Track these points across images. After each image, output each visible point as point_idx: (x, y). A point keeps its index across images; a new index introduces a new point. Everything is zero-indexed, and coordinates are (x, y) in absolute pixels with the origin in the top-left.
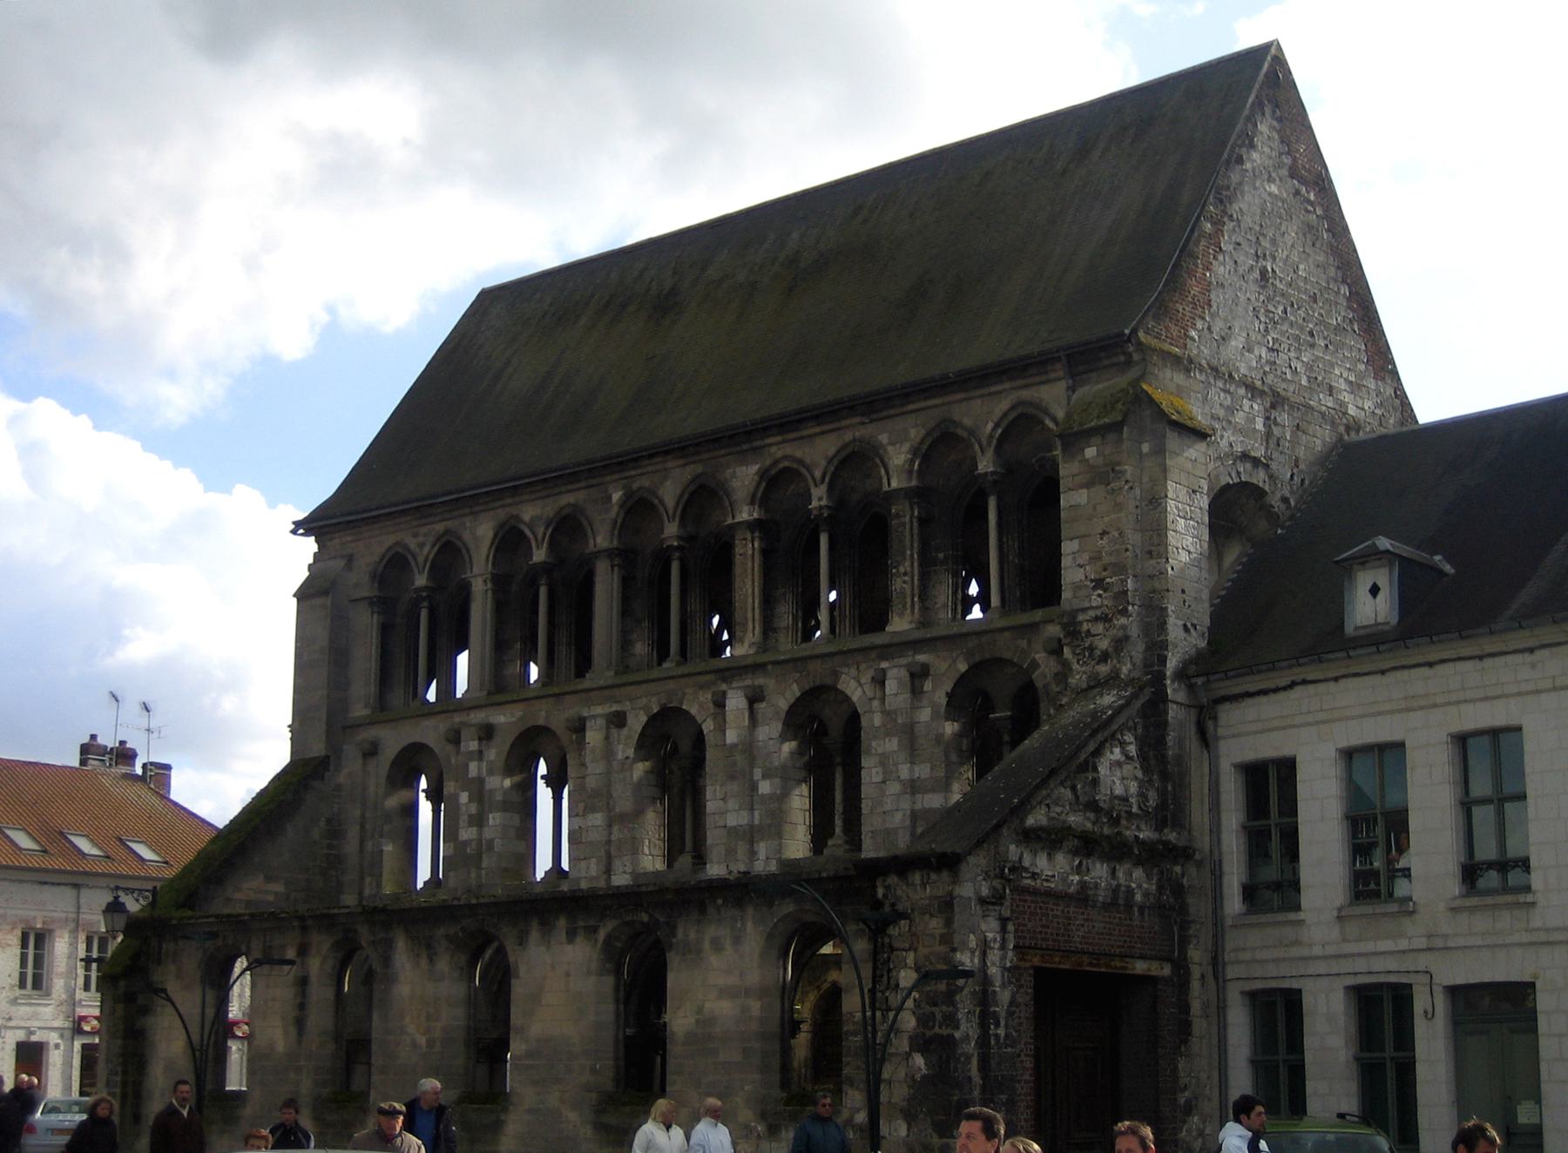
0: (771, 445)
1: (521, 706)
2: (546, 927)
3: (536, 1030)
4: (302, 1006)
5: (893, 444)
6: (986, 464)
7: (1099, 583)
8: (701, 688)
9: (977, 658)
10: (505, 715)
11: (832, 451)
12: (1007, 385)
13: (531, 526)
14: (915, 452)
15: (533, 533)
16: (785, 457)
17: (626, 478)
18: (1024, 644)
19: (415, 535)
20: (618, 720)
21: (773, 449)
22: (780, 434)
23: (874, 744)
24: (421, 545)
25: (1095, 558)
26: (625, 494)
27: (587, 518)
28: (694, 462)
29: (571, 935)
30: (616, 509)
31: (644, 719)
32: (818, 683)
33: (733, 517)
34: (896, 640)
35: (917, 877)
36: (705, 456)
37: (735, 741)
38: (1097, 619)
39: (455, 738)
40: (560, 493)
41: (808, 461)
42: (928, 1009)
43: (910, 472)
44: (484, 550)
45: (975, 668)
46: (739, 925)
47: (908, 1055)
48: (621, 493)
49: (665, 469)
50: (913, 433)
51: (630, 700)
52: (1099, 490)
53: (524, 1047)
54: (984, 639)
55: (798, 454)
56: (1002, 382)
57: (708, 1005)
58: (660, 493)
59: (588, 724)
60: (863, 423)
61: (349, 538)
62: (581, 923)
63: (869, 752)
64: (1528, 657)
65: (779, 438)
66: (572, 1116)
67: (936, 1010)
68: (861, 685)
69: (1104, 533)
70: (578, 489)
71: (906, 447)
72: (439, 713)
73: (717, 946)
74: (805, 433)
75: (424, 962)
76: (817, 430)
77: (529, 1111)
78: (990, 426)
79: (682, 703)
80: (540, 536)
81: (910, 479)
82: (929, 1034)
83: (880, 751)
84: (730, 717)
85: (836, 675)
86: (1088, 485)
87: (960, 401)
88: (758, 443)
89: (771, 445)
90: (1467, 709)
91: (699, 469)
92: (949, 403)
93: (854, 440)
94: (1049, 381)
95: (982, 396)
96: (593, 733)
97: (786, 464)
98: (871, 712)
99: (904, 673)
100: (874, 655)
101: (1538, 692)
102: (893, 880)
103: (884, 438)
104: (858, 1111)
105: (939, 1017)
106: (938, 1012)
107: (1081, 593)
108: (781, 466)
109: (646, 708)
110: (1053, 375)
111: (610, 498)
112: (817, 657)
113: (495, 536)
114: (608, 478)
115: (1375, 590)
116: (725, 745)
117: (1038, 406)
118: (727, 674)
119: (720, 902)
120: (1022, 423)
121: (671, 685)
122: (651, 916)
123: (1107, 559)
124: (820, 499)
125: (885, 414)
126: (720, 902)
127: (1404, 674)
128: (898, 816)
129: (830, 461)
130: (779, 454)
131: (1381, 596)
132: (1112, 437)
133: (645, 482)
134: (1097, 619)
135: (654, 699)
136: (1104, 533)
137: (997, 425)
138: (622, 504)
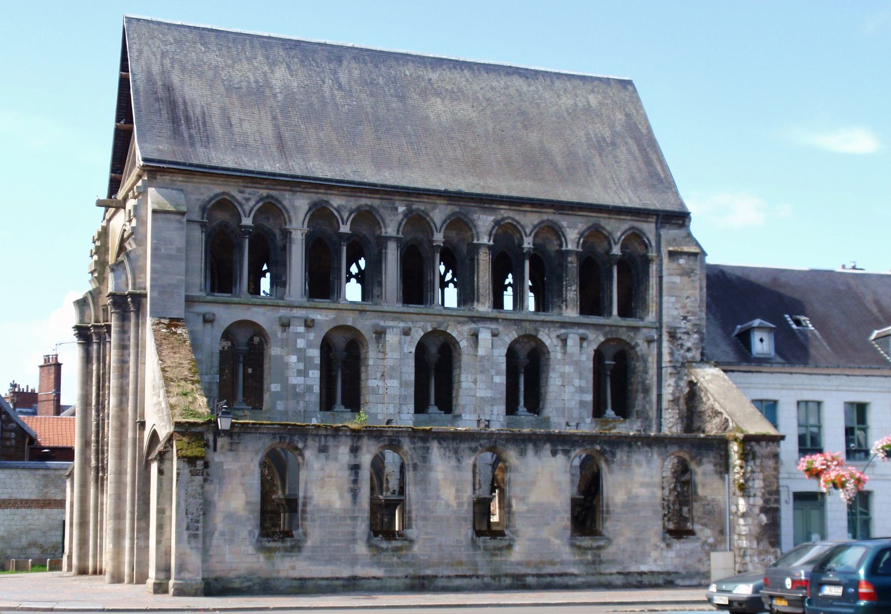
0: (500, 209)
1: (335, 312)
2: (537, 450)
3: (533, 498)
4: (355, 481)
5: (570, 228)
6: (616, 250)
7: (685, 318)
8: (459, 323)
9: (610, 336)
10: (321, 315)
11: (536, 222)
12: (628, 218)
13: (338, 210)
14: (581, 235)
15: (340, 214)
16: (508, 218)
17: (409, 201)
18: (632, 334)
19: (242, 192)
20: (406, 332)
21: (502, 212)
22: (509, 205)
23: (557, 367)
24: (248, 200)
25: (684, 307)
26: (407, 209)
27: (380, 215)
28: (454, 205)
29: (554, 453)
30: (401, 217)
31: (422, 334)
32: (528, 333)
33: (478, 240)
34: (567, 320)
35: (764, 443)
36: (462, 203)
37: (484, 354)
38: (685, 333)
39: (285, 325)
40: (362, 197)
41: (522, 223)
42: (768, 496)
43: (578, 243)
44: (301, 216)
45: (607, 341)
46: (650, 455)
47: (758, 515)
48: (405, 208)
49: (436, 204)
50: (580, 225)
51: (412, 322)
52: (685, 279)
53: (525, 508)
54: (613, 328)
55: (517, 218)
56: (628, 215)
57: (634, 490)
58: (431, 215)
59: (388, 331)
60: (554, 213)
61: (180, 179)
62: (560, 448)
63: (554, 370)
64: (827, 377)
65: (507, 207)
66: (557, 542)
67: (771, 497)
68: (550, 338)
69: (688, 297)
70: (374, 198)
71: (576, 231)
72: (270, 305)
73: (638, 464)
74: (522, 209)
75: (453, 462)
76: (529, 209)
77: (529, 540)
78: (619, 234)
79: (447, 329)
80: (345, 217)
81: (578, 247)
82: (768, 506)
83: (561, 370)
84: (480, 342)
85: (537, 331)
86: (681, 275)
87: (605, 218)
88: (494, 206)
89: (500, 209)
90: (805, 392)
91: (457, 209)
92: (599, 217)
93: (548, 220)
94: (647, 222)
95: (616, 219)
96: (391, 336)
97: (510, 221)
98: (556, 351)
99: (577, 338)
100: (558, 325)
101: (831, 390)
102: (753, 444)
103: (564, 224)
104: (709, 537)
105: (773, 500)
106: (773, 497)
107: (678, 320)
108: (507, 221)
109: (423, 328)
110: (649, 220)
111: (396, 209)
112: (526, 320)
113: (310, 209)
114: (397, 198)
115: (761, 340)
116: (476, 355)
117: (641, 231)
118: (475, 319)
119: (639, 444)
120: (636, 236)
121: (439, 319)
122: (601, 447)
123: (689, 309)
124: (529, 244)
125: (567, 212)
126: (639, 444)
127: (780, 375)
128: (573, 403)
129: (535, 227)
130: (506, 215)
131: (765, 343)
132: (692, 258)
133: (422, 207)
134: (685, 333)
135: (429, 324)
136: (688, 297)
137: (622, 235)
138: (406, 215)
